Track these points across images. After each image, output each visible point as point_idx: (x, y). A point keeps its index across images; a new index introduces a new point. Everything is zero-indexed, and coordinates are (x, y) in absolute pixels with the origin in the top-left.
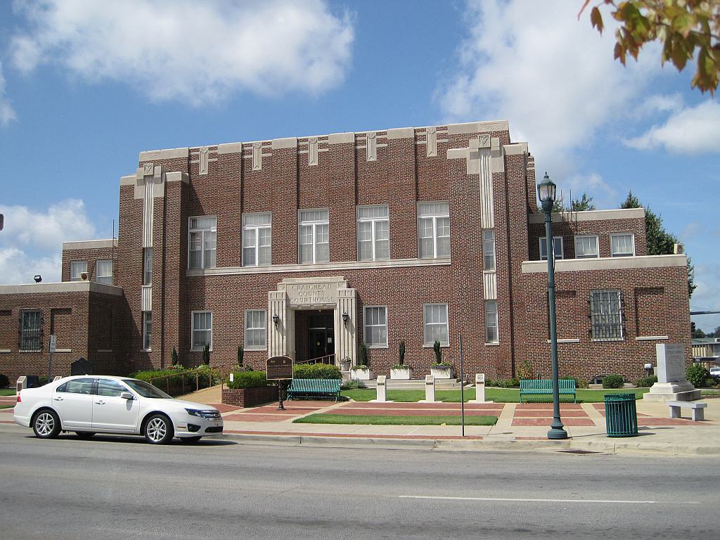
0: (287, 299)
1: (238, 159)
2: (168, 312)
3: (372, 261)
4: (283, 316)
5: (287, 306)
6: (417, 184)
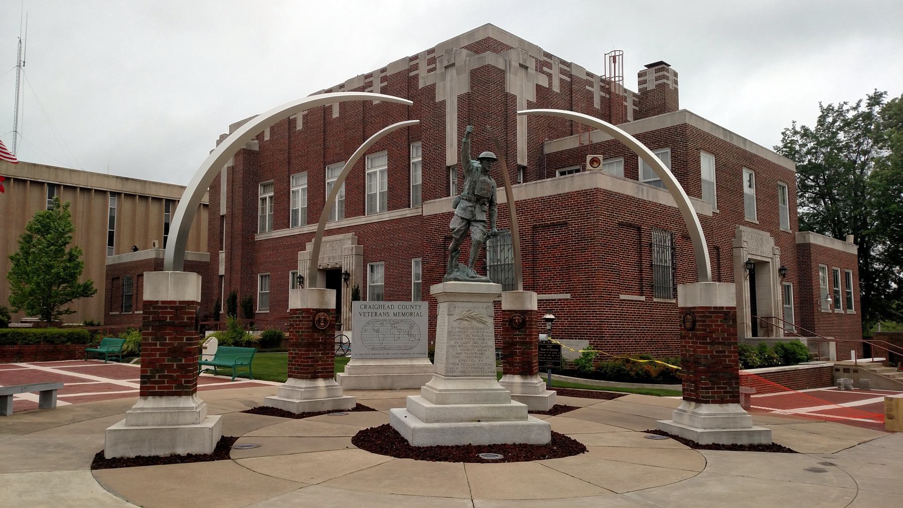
3: (378, 214)
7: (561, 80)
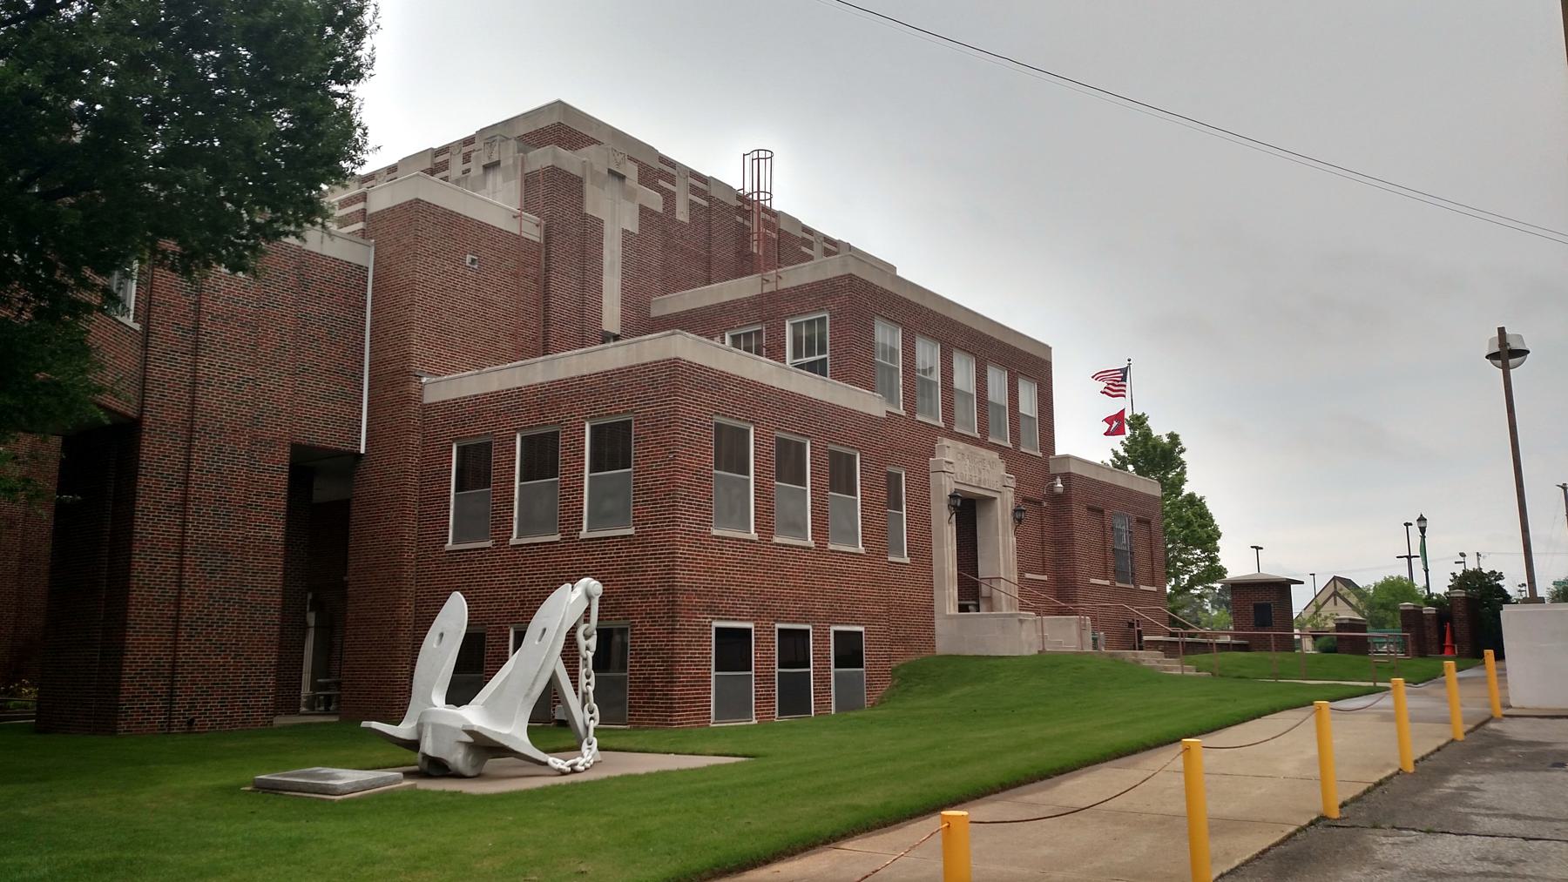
7: (692, 204)
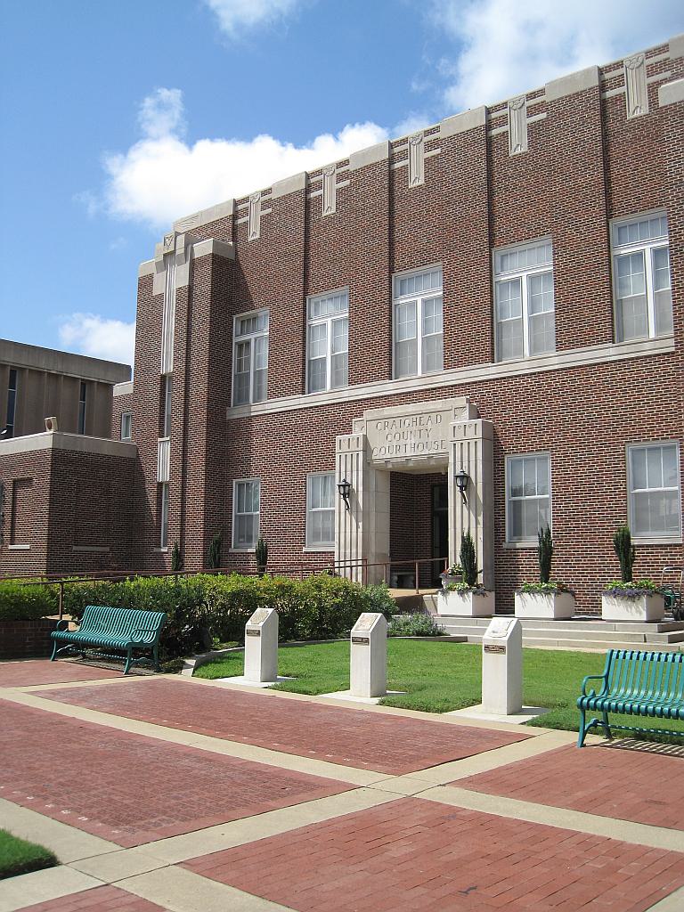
0: (367, 449)
1: (300, 200)
2: (190, 482)
4: (357, 482)
5: (368, 463)
6: (607, 182)
